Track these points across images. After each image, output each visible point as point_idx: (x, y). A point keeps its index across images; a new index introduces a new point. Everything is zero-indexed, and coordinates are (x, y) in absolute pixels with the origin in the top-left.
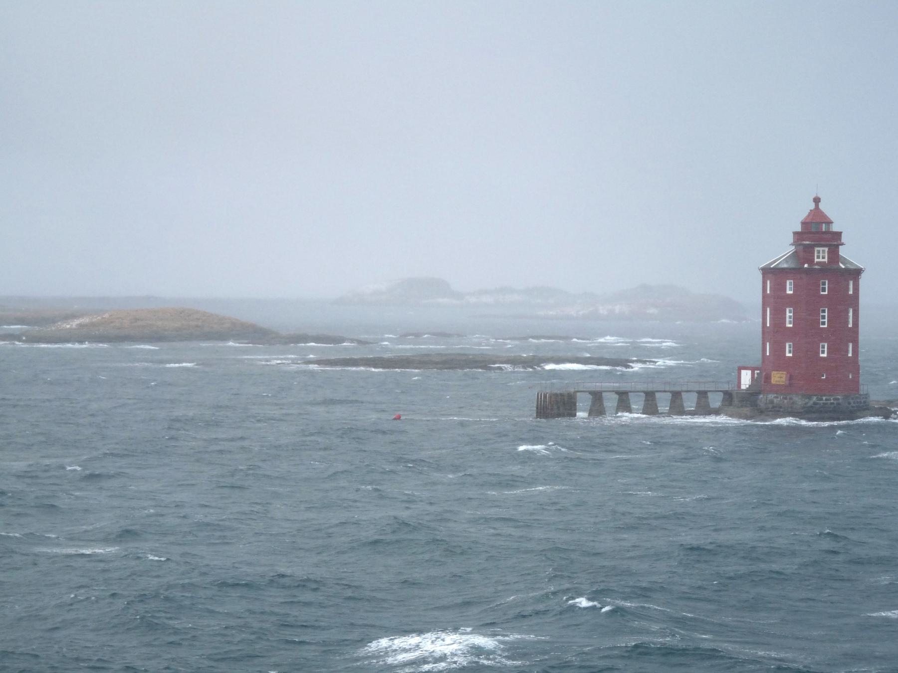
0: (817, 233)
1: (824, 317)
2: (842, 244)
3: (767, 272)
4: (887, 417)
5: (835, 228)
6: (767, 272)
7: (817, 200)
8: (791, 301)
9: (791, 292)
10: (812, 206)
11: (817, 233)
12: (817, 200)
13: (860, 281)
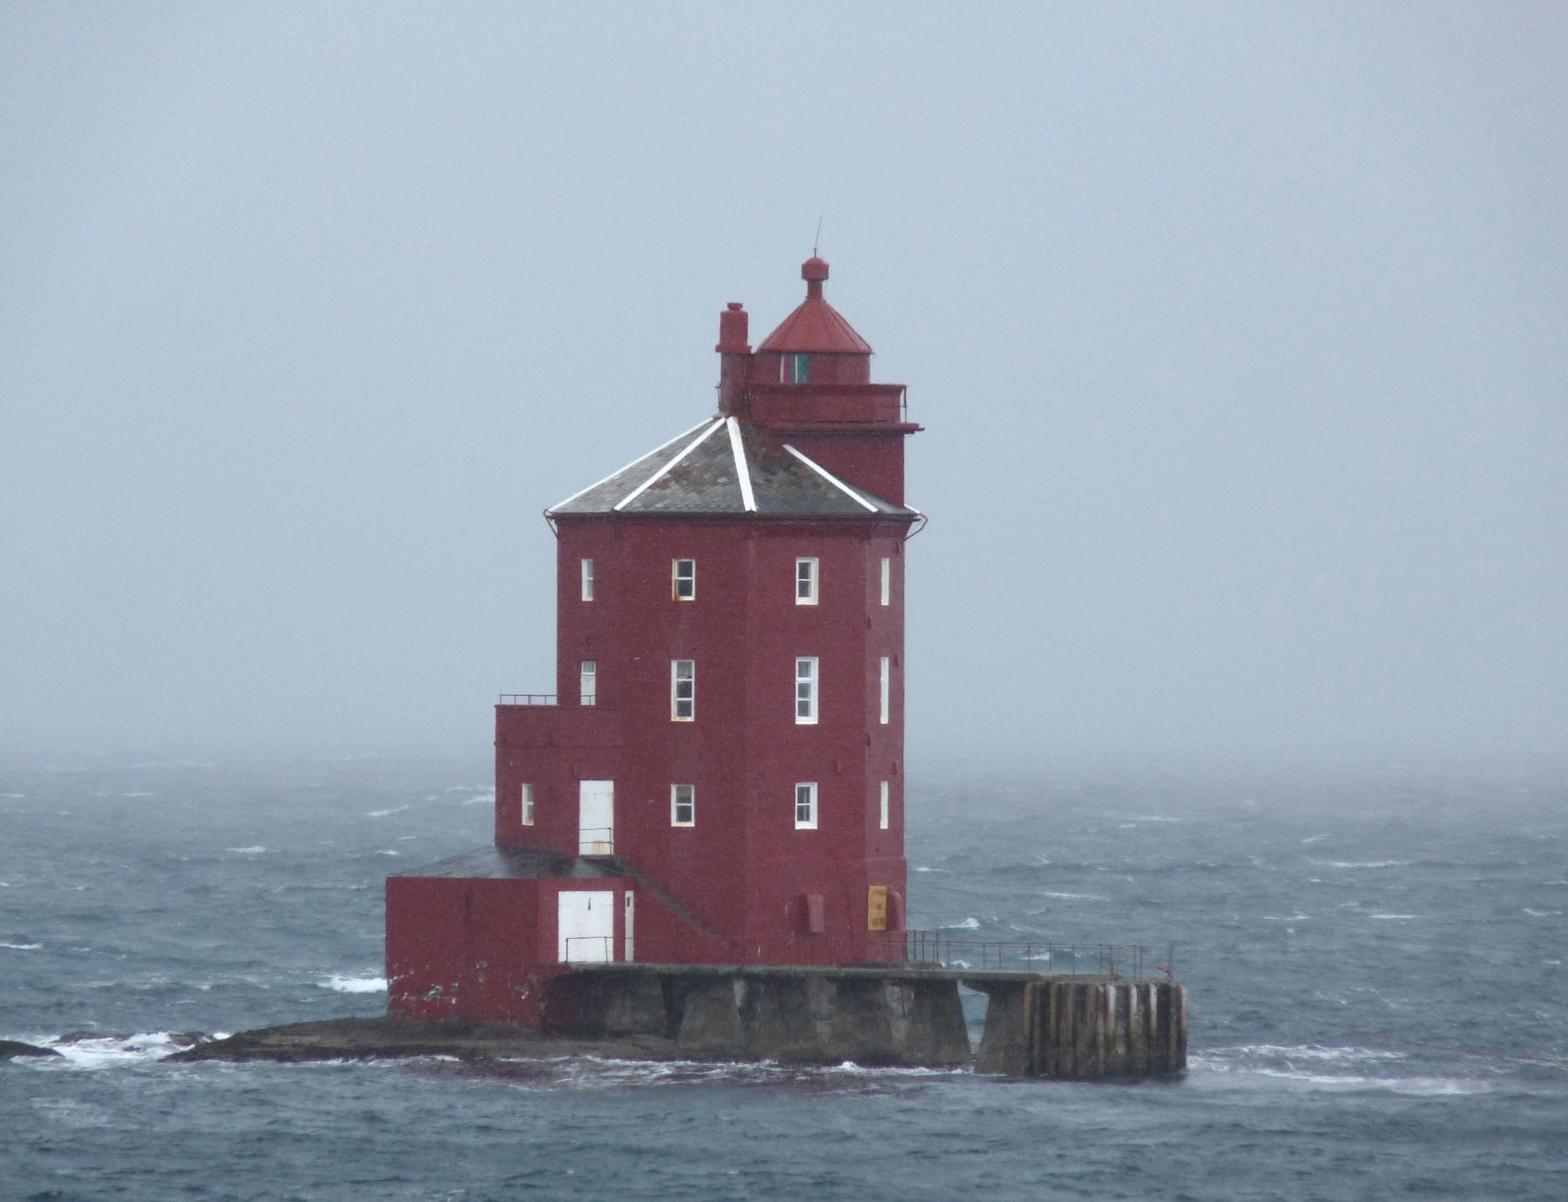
0: (811, 395)
1: (684, 690)
2: (912, 429)
3: (577, 531)
4: (741, 1011)
5: (879, 374)
6: (577, 531)
7: (815, 273)
8: (805, 632)
9: (590, 599)
10: (798, 292)
11: (811, 395)
12: (815, 273)
13: (908, 544)
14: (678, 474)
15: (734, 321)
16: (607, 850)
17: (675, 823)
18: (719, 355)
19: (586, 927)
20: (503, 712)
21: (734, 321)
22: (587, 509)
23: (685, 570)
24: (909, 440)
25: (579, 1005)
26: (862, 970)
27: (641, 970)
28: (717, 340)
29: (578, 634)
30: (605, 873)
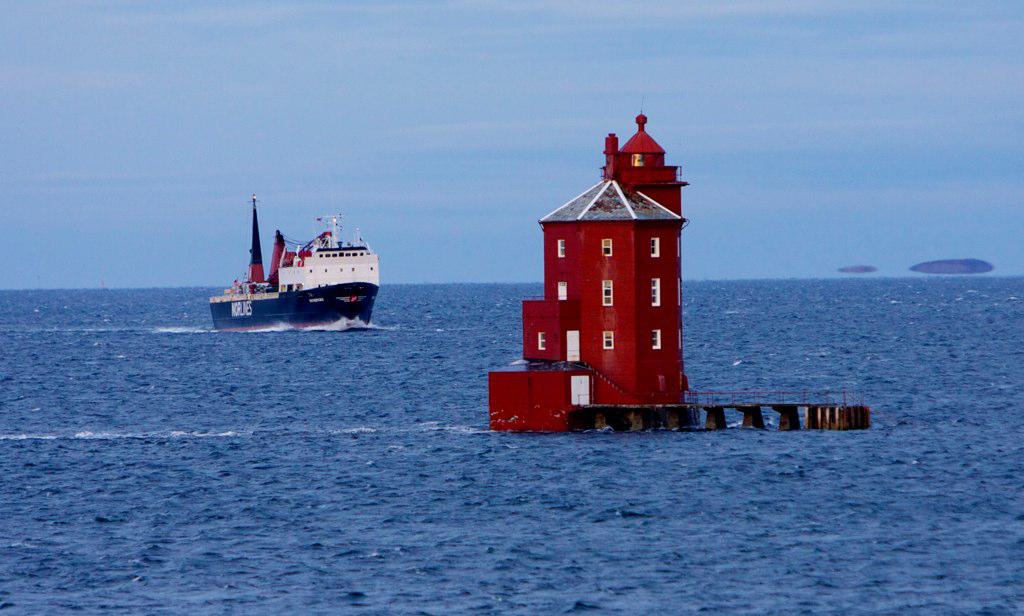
0: (642, 168)
1: (608, 293)
3: (553, 229)
5: (668, 163)
6: (553, 229)
7: (642, 121)
12: (642, 121)
14: (598, 205)
15: (612, 140)
16: (577, 359)
17: (605, 348)
18: (604, 156)
19: (580, 390)
20: (526, 304)
21: (612, 140)
22: (551, 220)
23: (607, 244)
24: (683, 188)
25: (580, 421)
26: (258, 331)
27: (594, 408)
28: (604, 149)
29: (554, 270)
30: (579, 369)
